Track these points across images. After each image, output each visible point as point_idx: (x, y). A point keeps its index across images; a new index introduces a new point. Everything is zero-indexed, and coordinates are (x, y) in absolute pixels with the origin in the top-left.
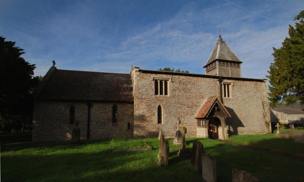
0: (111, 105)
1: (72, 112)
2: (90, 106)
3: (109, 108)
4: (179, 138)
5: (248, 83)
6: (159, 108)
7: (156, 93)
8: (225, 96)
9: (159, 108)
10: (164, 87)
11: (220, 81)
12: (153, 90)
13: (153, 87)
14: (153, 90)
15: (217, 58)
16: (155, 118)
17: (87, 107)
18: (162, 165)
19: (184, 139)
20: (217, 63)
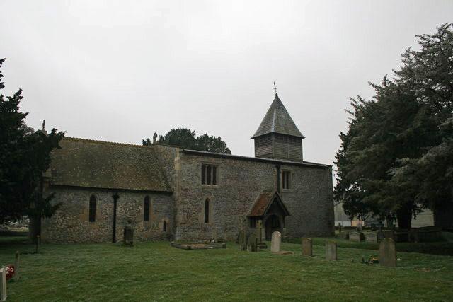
0: (143, 197)
1: (93, 205)
2: (116, 198)
3: (140, 199)
4: (398, 253)
5: (310, 171)
6: (207, 202)
7: (203, 183)
8: (283, 188)
9: (207, 202)
10: (212, 174)
11: (278, 168)
12: (199, 177)
13: (200, 174)
14: (199, 177)
15: (272, 131)
16: (202, 216)
17: (112, 199)
18: (352, 133)
19: (369, 248)
20: (273, 137)
